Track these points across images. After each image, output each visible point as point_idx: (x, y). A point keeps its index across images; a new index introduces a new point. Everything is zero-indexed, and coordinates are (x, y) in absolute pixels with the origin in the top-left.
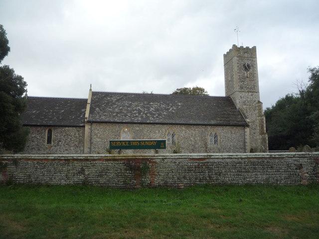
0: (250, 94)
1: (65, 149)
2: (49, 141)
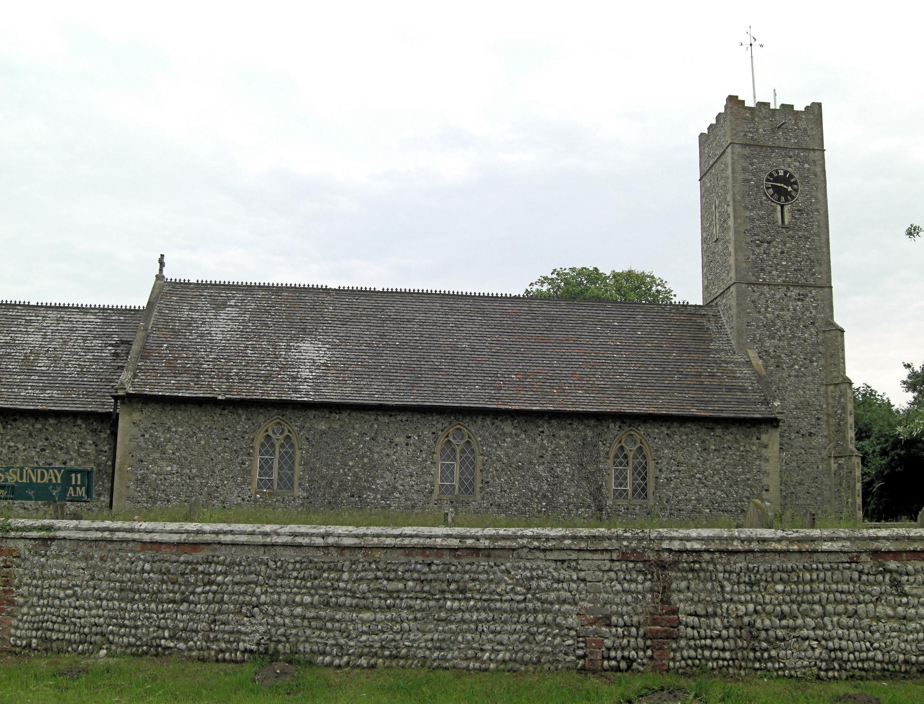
0: (794, 292)
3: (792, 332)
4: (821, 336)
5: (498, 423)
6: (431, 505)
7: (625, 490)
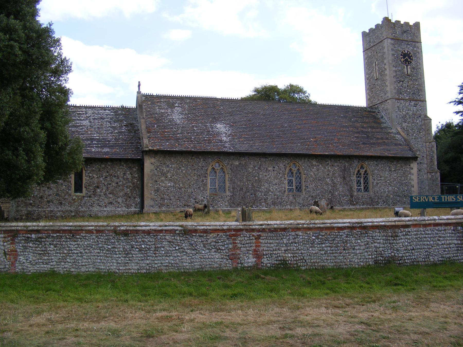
0: (413, 103)
1: (106, 201)
2: (78, 188)
3: (413, 120)
4: (423, 122)
5: (310, 160)
6: (285, 197)
7: (292, 188)
